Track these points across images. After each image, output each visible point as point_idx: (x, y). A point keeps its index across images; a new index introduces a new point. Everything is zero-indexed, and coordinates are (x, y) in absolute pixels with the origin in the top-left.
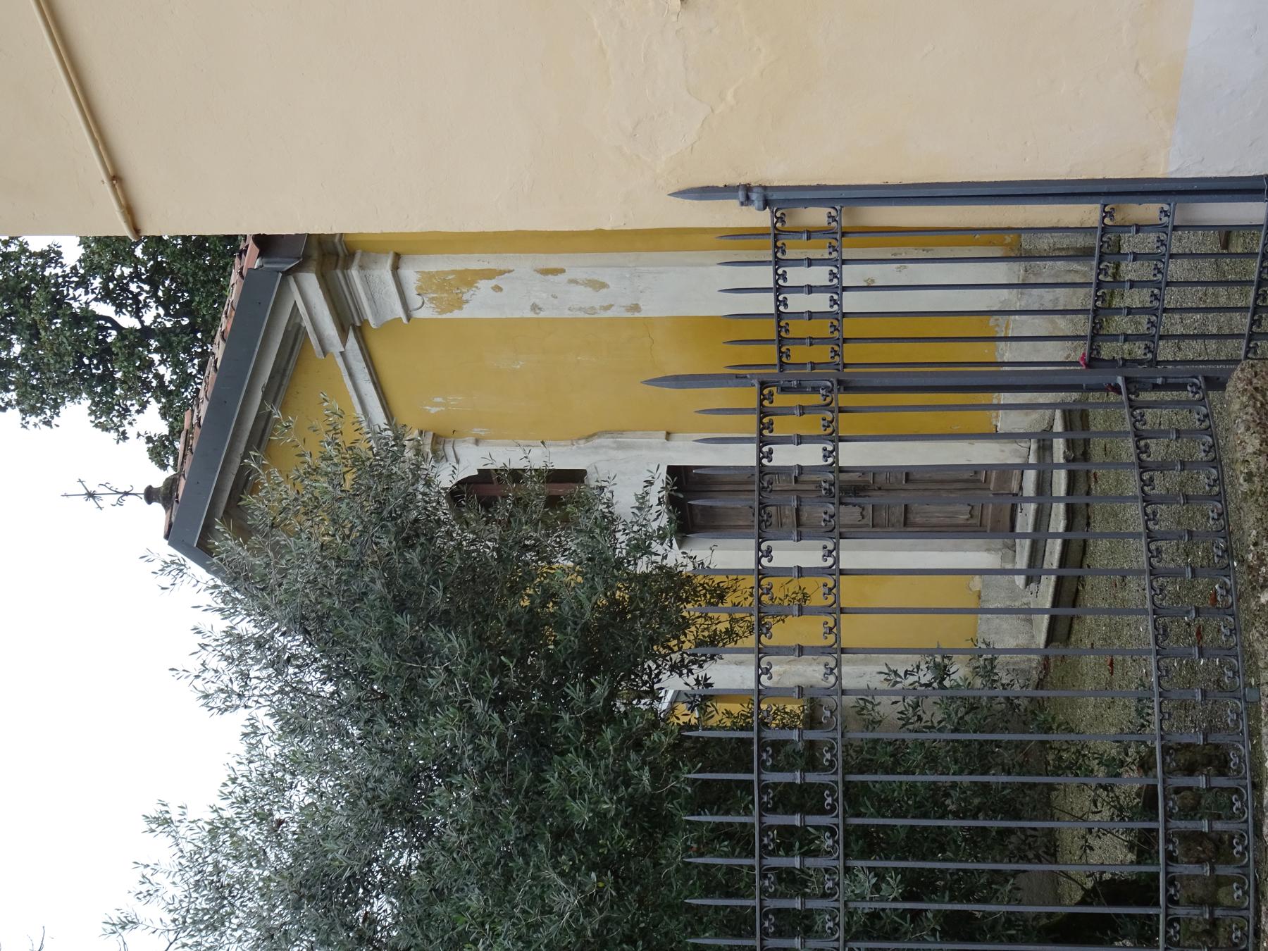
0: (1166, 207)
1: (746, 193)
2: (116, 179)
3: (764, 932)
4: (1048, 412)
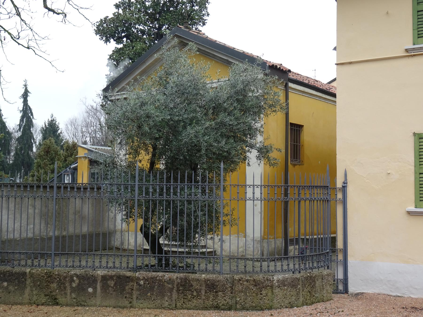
0: (342, 261)
1: (345, 183)
2: (350, 63)
3: (167, 185)
4: (213, 247)
